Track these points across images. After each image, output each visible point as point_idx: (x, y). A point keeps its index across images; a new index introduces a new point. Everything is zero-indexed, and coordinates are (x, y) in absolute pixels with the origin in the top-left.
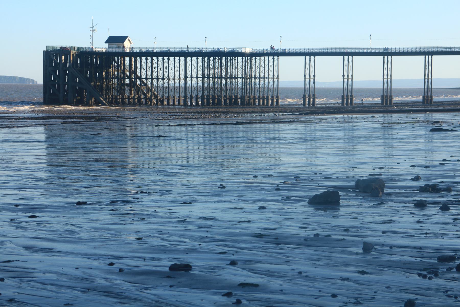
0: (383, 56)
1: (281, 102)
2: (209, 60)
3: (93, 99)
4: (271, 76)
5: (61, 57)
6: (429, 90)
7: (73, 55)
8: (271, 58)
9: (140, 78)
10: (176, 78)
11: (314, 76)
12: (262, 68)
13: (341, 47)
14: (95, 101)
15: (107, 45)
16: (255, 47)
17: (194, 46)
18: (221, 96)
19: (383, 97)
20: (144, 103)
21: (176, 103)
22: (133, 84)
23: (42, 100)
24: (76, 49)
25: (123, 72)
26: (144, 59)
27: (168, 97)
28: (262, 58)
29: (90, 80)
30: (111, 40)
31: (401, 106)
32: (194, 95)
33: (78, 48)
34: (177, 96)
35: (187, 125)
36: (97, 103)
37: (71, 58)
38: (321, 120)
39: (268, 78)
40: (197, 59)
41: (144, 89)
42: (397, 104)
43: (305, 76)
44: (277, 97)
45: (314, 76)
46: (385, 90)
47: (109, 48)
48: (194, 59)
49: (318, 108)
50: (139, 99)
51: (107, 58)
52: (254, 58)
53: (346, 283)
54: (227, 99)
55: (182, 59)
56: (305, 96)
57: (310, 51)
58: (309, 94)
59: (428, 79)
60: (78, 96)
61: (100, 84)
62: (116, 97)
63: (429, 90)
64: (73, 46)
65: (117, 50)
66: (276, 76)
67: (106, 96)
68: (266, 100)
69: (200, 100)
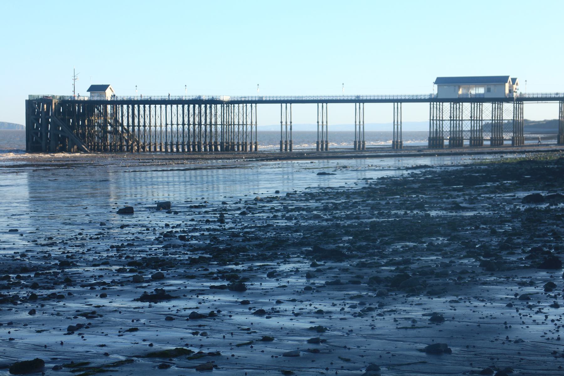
0: (393, 104)
1: (260, 148)
2: (200, 107)
3: (75, 147)
4: (249, 123)
5: (43, 106)
6: (289, 134)
7: (55, 104)
8: (249, 105)
9: (122, 125)
10: (157, 125)
11: (291, 122)
12: (241, 115)
13: (388, 94)
14: (78, 148)
15: (89, 94)
16: (233, 95)
17: (175, 95)
18: (201, 143)
19: (355, 142)
20: (126, 150)
21: (158, 149)
22: (115, 132)
23: (25, 149)
24: (58, 98)
25: (105, 120)
26: (125, 106)
27: (150, 144)
28: (241, 105)
29: (72, 127)
30: (93, 89)
31: (406, 150)
32: (175, 142)
33: (60, 97)
34: (158, 141)
35: (135, 171)
36: (80, 150)
37: (53, 107)
38: (266, 165)
39: (246, 125)
40: (177, 106)
41: (125, 136)
42: (369, 150)
43: (281, 122)
44: (256, 143)
45: (291, 122)
46: (320, 135)
47: (91, 96)
48: (174, 106)
49: (294, 153)
50: (121, 146)
51: (89, 106)
52: (208, 106)
53: (104, 348)
54: (196, 145)
55: (163, 106)
56: (281, 142)
57: (315, 98)
58: (322, 138)
59: (397, 124)
60: (61, 144)
61: (82, 132)
62: (98, 143)
63: (289, 134)
64: (55, 95)
65: (98, 99)
66: (254, 123)
67: (88, 144)
68: (196, 146)
69: (180, 147)
